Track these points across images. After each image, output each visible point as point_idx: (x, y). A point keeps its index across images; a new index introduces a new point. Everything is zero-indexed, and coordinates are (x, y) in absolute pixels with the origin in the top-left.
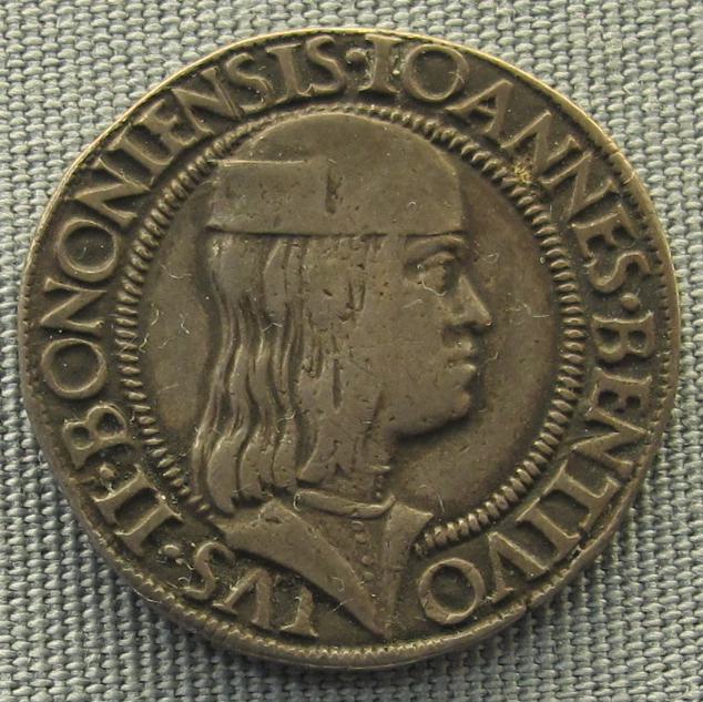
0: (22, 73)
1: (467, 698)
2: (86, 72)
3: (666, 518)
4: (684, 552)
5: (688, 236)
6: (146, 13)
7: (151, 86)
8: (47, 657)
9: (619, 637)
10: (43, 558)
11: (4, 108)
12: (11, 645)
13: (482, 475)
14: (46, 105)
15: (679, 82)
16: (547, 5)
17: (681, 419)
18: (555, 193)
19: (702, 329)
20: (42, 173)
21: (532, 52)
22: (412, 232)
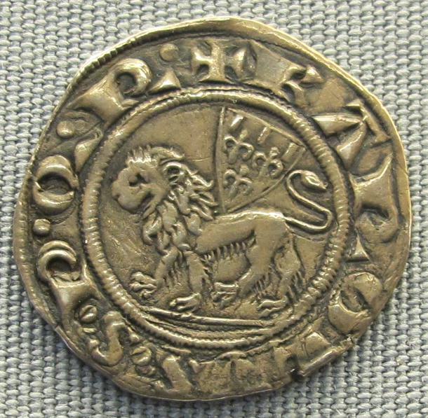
0: (141, 9)
1: (270, 415)
2: (112, 17)
3: (404, 342)
4: (403, 352)
5: (70, 20)
6: (37, 12)
7: (132, 31)
8: (55, 384)
9: (354, 389)
10: (55, 377)
11: (3, 108)
12: (42, 96)
13: (243, 236)
14: (58, 43)
15: (132, 16)
16: (129, 4)
17: (419, 283)
18: (389, 135)
19: (427, 218)
20: (52, 90)
21: (154, 12)
22: (375, 201)
